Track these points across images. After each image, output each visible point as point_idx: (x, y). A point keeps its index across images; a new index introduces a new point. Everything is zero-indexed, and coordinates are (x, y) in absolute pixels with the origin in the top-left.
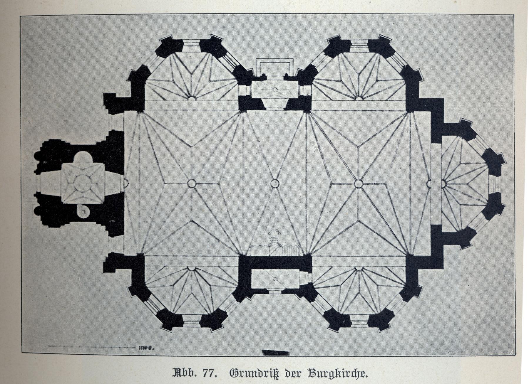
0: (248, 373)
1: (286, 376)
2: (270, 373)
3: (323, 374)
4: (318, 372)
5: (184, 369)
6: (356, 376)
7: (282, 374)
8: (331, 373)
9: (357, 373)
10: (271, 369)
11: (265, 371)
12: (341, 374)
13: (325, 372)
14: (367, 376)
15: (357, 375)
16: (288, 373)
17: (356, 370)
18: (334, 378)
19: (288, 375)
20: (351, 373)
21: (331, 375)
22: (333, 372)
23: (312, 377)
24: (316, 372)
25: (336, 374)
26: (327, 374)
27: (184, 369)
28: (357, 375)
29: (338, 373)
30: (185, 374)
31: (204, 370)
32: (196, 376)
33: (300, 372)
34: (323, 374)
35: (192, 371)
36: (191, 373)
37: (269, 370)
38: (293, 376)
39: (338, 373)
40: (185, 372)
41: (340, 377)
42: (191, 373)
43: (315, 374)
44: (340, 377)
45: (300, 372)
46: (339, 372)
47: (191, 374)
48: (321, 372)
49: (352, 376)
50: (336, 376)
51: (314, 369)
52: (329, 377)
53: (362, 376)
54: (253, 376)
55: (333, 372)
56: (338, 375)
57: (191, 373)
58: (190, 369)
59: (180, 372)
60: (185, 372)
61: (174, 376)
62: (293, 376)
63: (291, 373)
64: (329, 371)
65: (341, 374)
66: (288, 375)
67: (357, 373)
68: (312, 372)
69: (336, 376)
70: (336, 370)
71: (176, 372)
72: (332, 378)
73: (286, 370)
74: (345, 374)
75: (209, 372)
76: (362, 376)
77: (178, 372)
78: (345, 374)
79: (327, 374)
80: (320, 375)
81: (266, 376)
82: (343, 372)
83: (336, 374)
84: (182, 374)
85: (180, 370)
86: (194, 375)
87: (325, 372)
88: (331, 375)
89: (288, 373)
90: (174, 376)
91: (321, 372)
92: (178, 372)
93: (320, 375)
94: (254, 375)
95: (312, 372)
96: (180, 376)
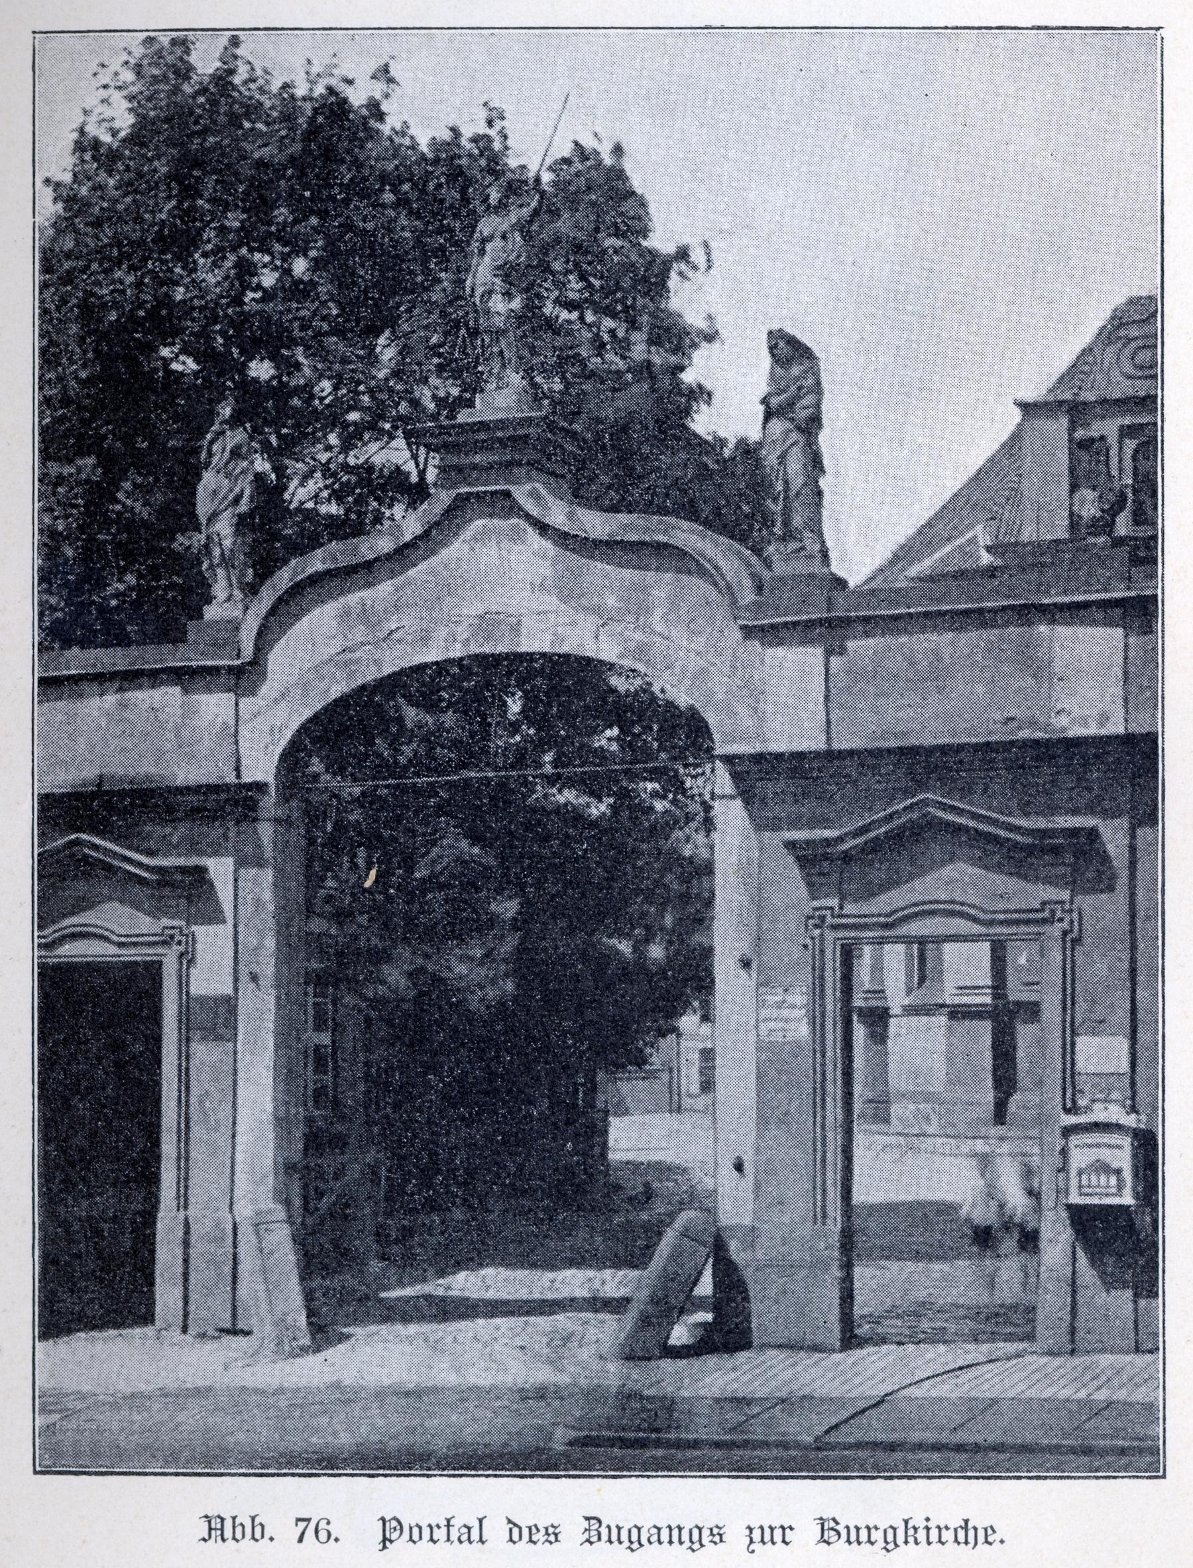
0: (767, 1532)
1: (511, 1540)
2: (444, 1530)
3: (778, 1534)
4: (847, 1527)
5: (234, 1518)
6: (966, 1543)
7: (496, 1531)
8: (890, 1532)
9: (971, 1533)
10: (928, 1519)
11: (430, 1526)
12: (921, 1535)
13: (868, 1528)
14: (1002, 1542)
15: (971, 1539)
16: (516, 1531)
17: (966, 1522)
18: (896, 1546)
19: (516, 1537)
20: (952, 1532)
21: (890, 1538)
22: (895, 1529)
23: (829, 1543)
24: (840, 1528)
25: (908, 1533)
26: (877, 1536)
27: (234, 1518)
28: (971, 1539)
29: (911, 1532)
30: (239, 1535)
31: (299, 1520)
32: (272, 1539)
33: (791, 1528)
34: (778, 1534)
35: (262, 1526)
36: (258, 1530)
37: (443, 1523)
38: (531, 1541)
39: (911, 1532)
40: (239, 1530)
41: (916, 1543)
42: (258, 1530)
43: (839, 1534)
44: (916, 1543)
45: (791, 1528)
46: (916, 1529)
47: (258, 1535)
48: (858, 1529)
49: (956, 1540)
50: (906, 1542)
51: (834, 1520)
52: (881, 1544)
53: (987, 1542)
54: (671, 1542)
55: (895, 1529)
56: (911, 1539)
57: (257, 1530)
58: (253, 1519)
59: (222, 1529)
60: (239, 1530)
61: (204, 1540)
62: (531, 1541)
63: (525, 1532)
64: (952, 1526)
65: (921, 1535)
66: (516, 1537)
67: (971, 1533)
68: (828, 1530)
69: (906, 1542)
70: (906, 1522)
71: (210, 1529)
72: (594, 1539)
73: (510, 1521)
74: (934, 1534)
75: (310, 1528)
76: (987, 1542)
77: (215, 1527)
78: (934, 1534)
79: (877, 1536)
80: (857, 1536)
81: (432, 1540)
82: (928, 1529)
83: (908, 1533)
84: (228, 1533)
85: (223, 1520)
86: (267, 1536)
87: (868, 1528)
88: (890, 1538)
89: (516, 1531)
90: (204, 1540)
91: (772, 1529)
92: (215, 1527)
93: (853, 1537)
94: (675, 1538)
95: (828, 1530)
96: (223, 1540)
